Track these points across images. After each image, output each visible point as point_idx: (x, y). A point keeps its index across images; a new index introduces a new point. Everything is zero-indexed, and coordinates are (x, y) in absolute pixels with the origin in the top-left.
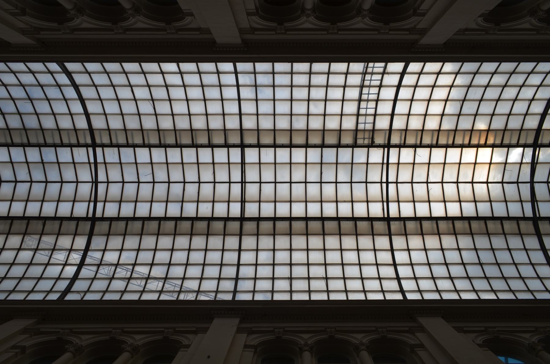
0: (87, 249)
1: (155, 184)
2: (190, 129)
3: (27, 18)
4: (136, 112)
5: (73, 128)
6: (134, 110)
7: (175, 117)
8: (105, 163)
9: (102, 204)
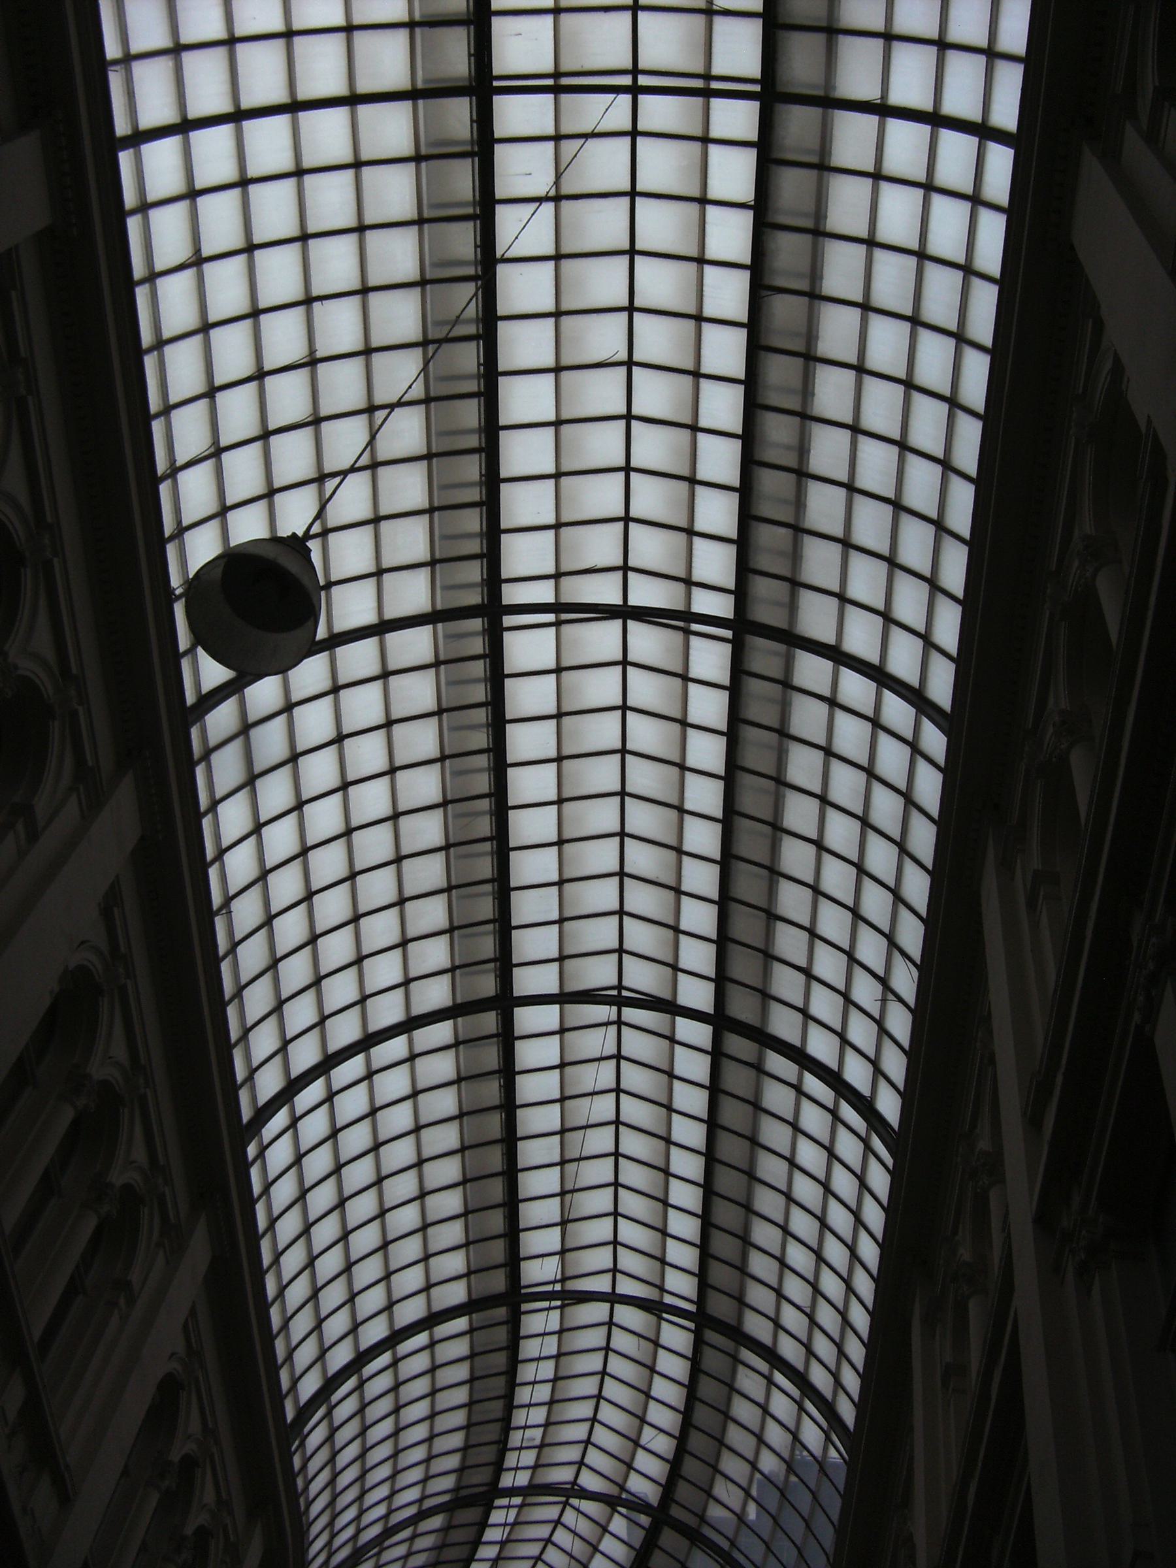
0: (836, 655)
1: (633, 464)
2: (424, 406)
4: (372, 581)
5: (461, 1187)
6: (345, 246)
7: (408, 892)
8: (557, 576)
9: (697, 593)
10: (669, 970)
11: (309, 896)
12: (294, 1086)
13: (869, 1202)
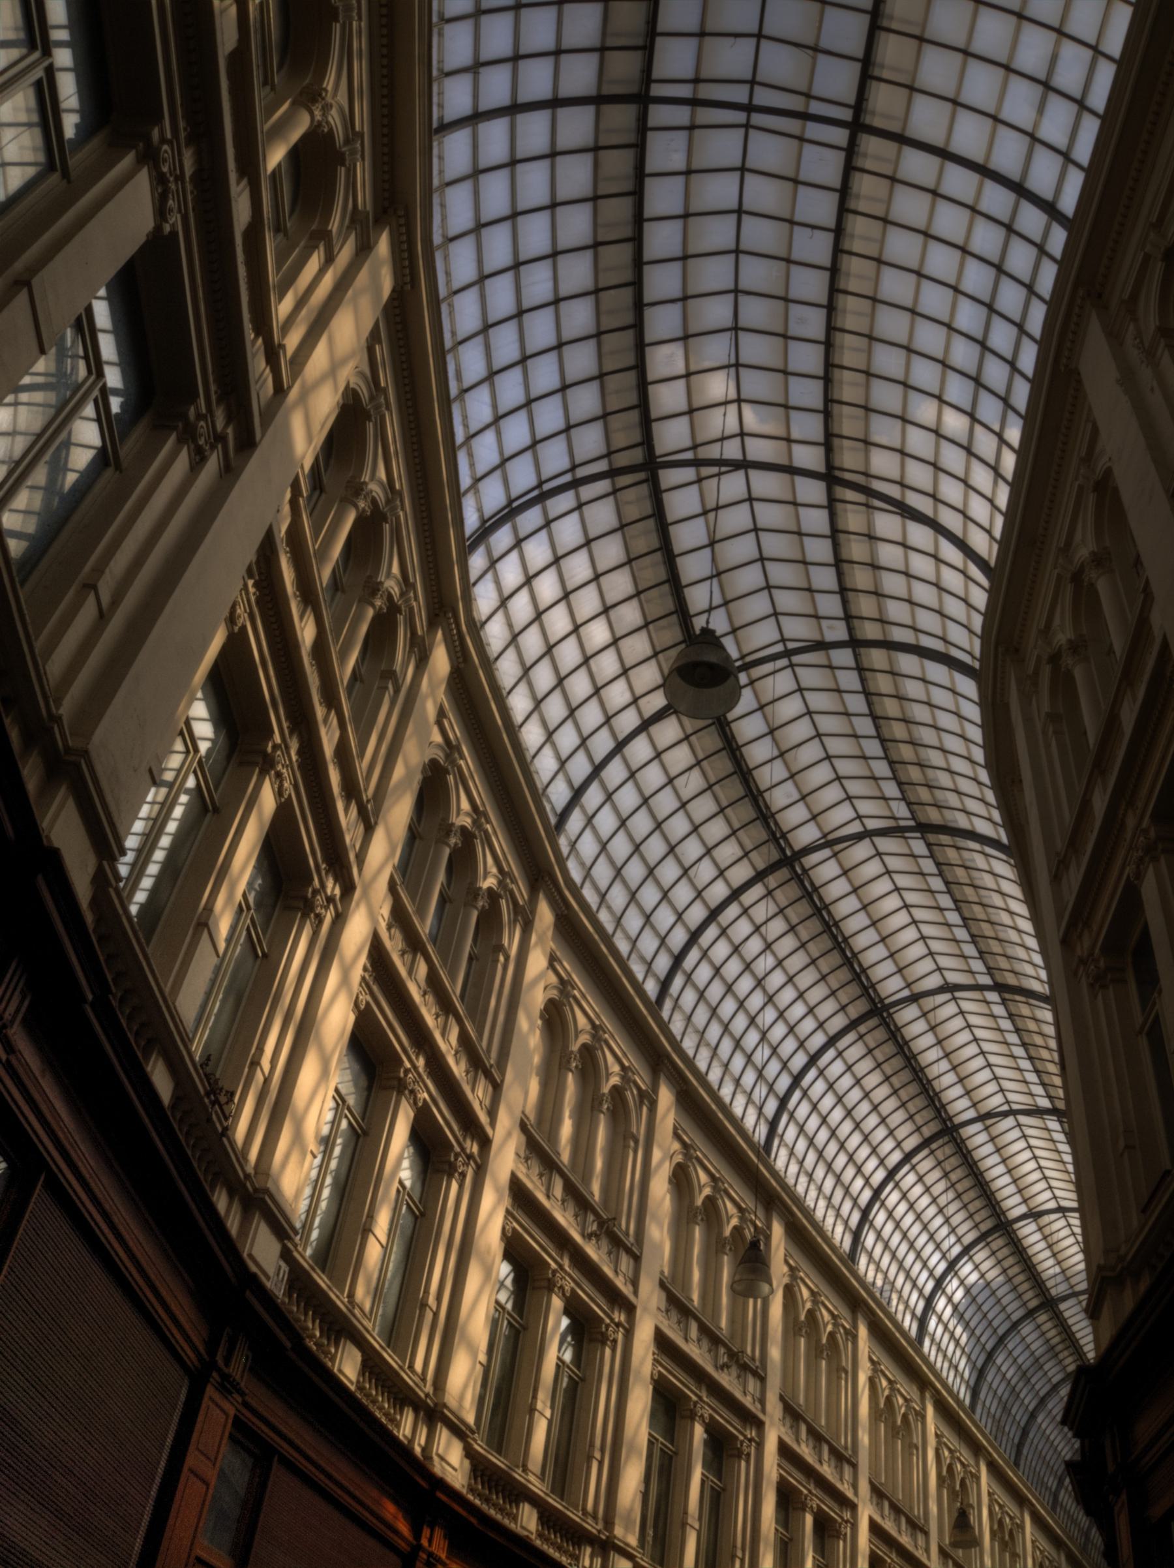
3: (397, 667)
10: (796, 536)
11: (623, 823)
12: (578, 794)
13: (1025, 937)
